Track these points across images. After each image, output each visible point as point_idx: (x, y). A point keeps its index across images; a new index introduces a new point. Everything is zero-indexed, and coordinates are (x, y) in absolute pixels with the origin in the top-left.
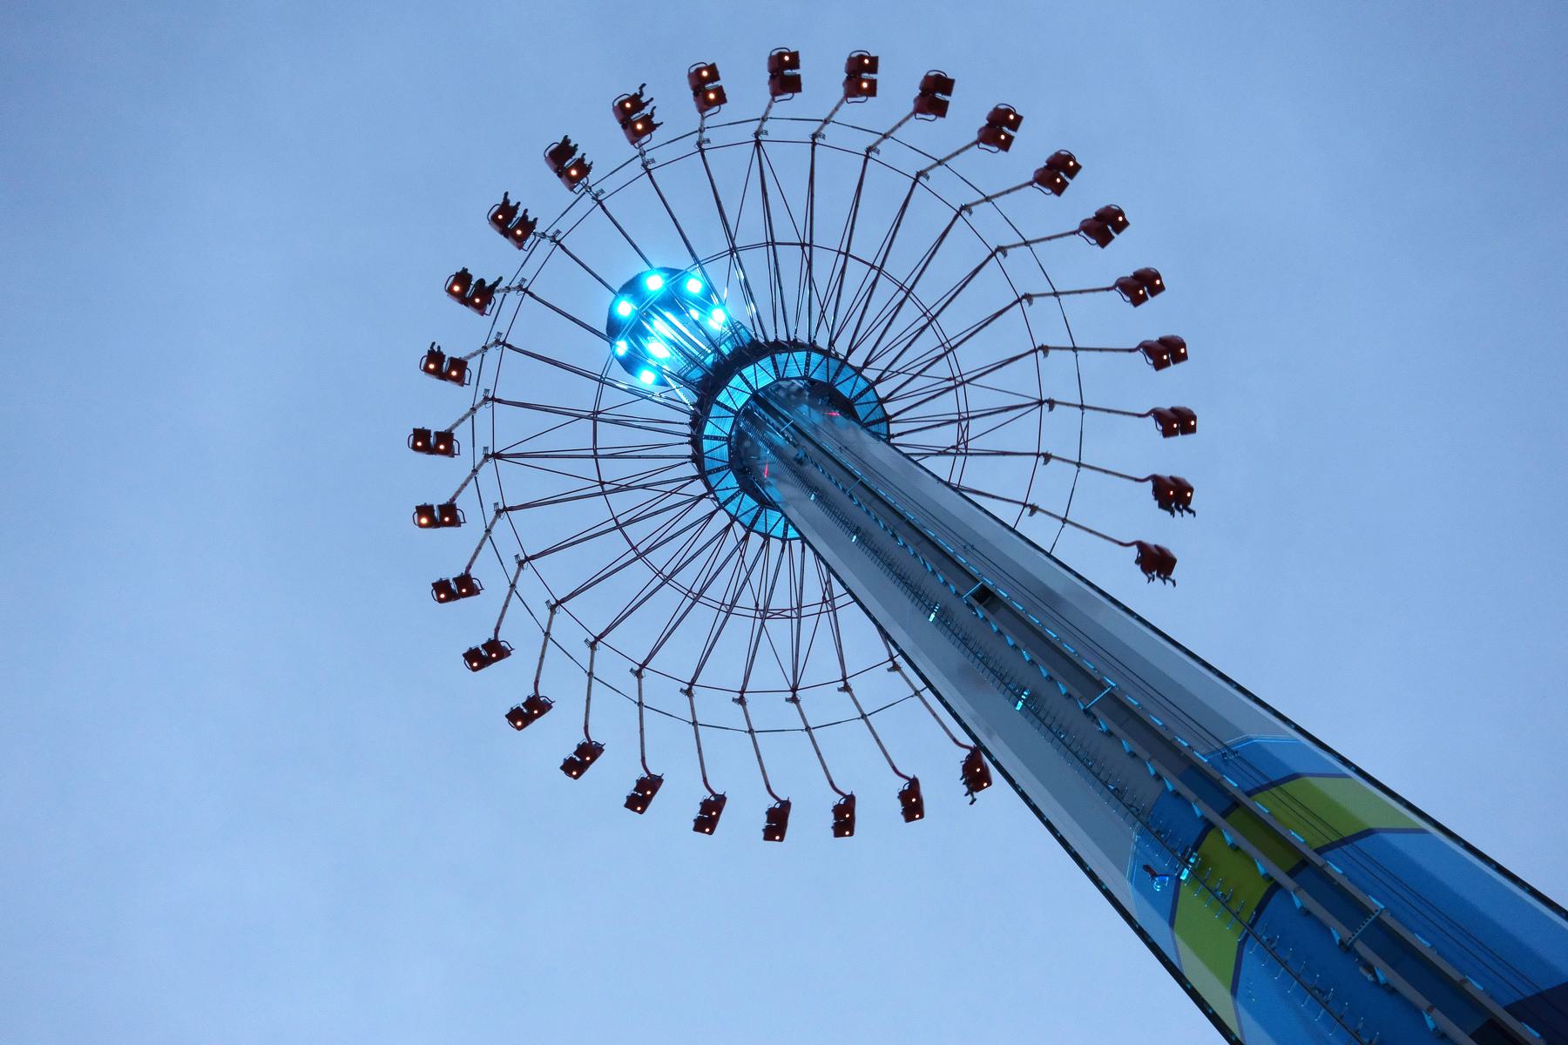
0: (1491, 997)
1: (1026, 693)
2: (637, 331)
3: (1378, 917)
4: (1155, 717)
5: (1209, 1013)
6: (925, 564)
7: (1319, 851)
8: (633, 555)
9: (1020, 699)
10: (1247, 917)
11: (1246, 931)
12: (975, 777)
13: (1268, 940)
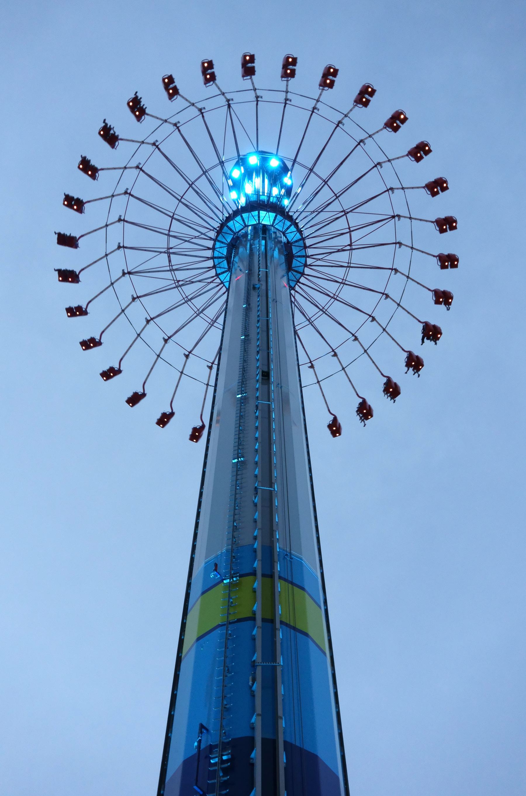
0: (284, 733)
1: (242, 459)
2: (249, 174)
3: (276, 666)
4: (278, 516)
5: (179, 655)
6: (258, 374)
7: (282, 622)
8: (167, 232)
9: (238, 459)
10: (232, 618)
11: (226, 623)
12: (196, 434)
13: (230, 634)
